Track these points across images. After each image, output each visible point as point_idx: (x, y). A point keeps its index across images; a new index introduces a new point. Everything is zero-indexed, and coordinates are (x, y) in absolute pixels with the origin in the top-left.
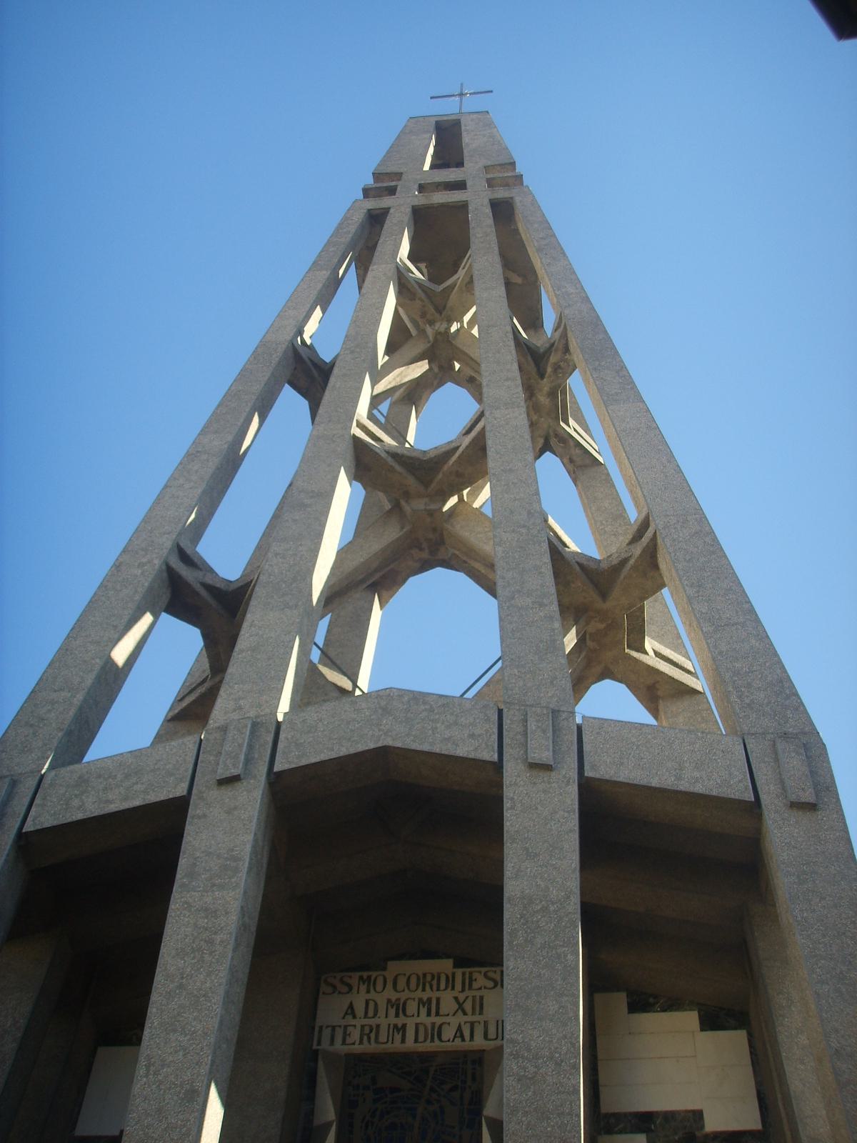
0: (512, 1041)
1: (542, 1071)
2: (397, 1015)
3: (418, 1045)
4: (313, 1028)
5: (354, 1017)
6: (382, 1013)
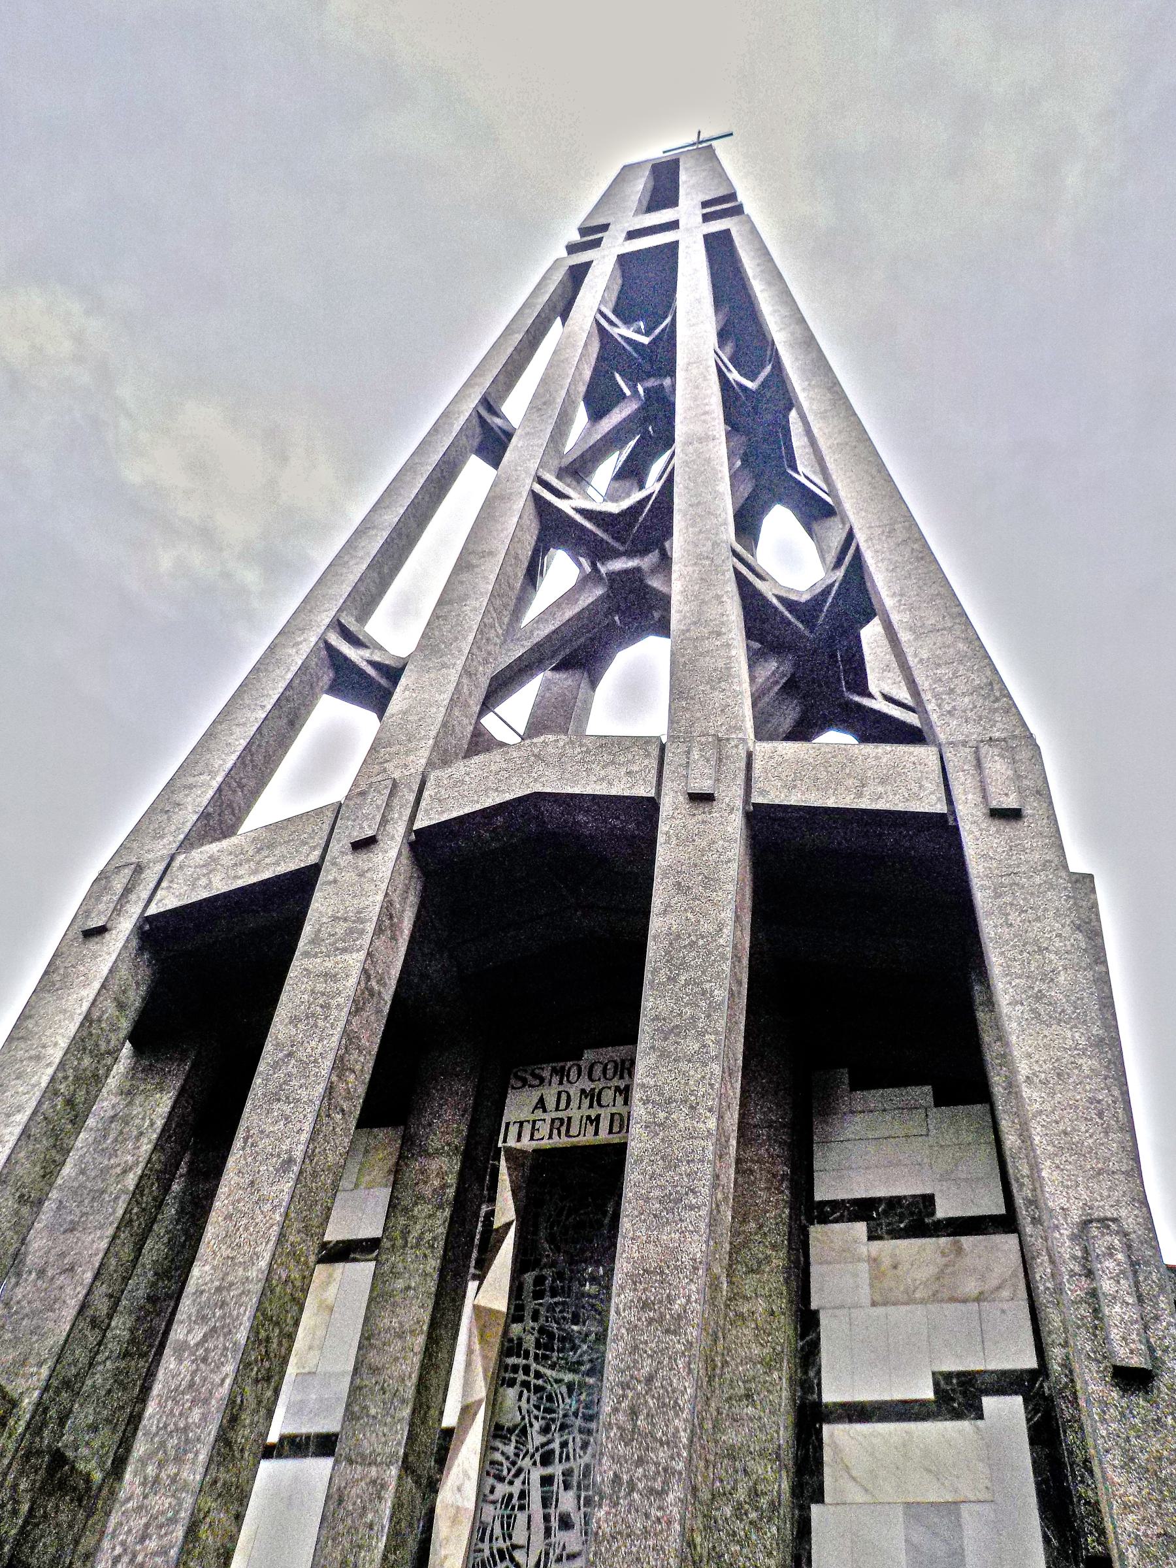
2: (591, 1106)
3: (611, 1136)
5: (545, 1111)
6: (574, 1104)
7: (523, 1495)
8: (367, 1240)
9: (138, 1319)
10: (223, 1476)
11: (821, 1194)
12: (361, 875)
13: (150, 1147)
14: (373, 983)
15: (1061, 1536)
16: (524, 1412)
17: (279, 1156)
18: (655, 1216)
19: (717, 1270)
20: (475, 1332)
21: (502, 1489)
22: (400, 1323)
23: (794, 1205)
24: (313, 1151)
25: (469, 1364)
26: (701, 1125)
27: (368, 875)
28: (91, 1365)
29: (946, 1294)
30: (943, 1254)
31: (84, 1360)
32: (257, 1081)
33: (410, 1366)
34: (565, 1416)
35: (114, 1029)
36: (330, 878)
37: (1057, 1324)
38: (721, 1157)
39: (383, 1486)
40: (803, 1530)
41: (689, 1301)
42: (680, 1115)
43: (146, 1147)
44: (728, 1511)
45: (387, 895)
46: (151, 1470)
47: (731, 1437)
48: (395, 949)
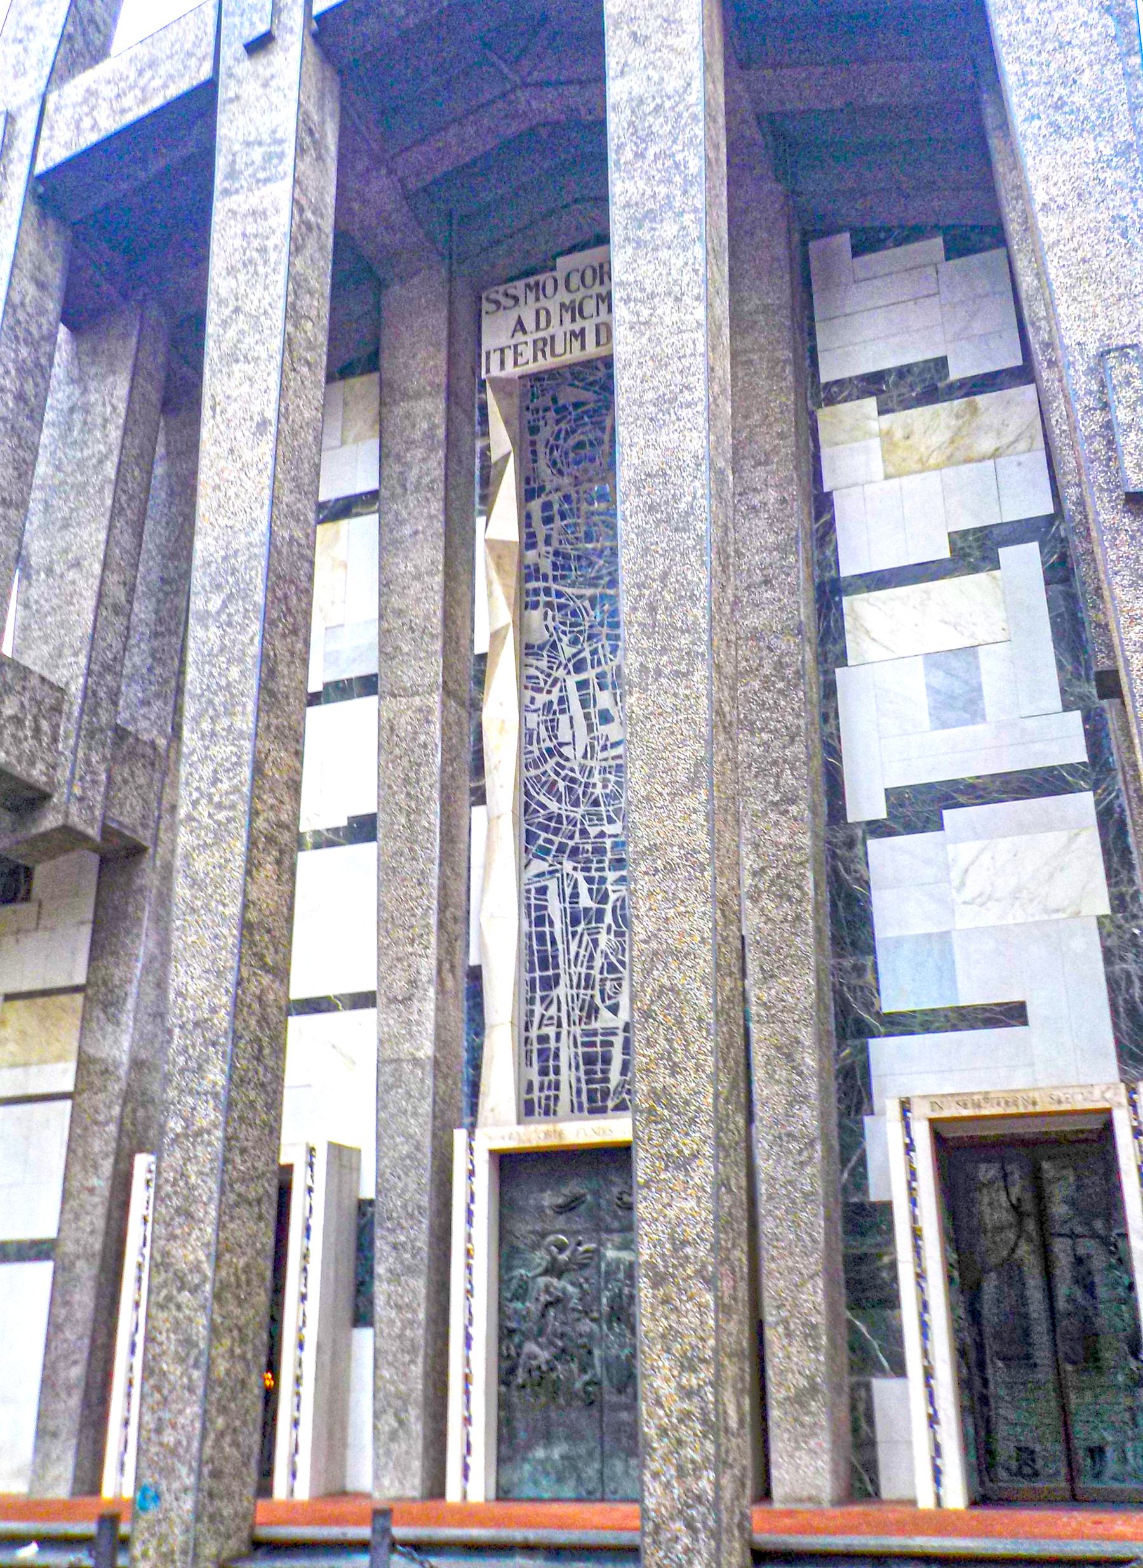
0: (622, 284)
1: (659, 312)
2: (573, 320)
4: (480, 356)
5: (525, 332)
6: (555, 320)
7: (562, 700)
8: (366, 494)
9: (159, 601)
10: (274, 721)
11: (826, 375)
12: (265, 85)
13: (119, 433)
14: (309, 215)
15: (1076, 660)
16: (551, 629)
17: (251, 418)
18: (651, 419)
19: (721, 464)
20: (492, 565)
21: (541, 699)
22: (415, 567)
23: (801, 396)
24: (287, 409)
25: (490, 595)
26: (688, 316)
27: (273, 83)
28: (125, 649)
29: (960, 455)
30: (957, 417)
31: (117, 645)
32: (210, 345)
33: (434, 604)
34: (591, 627)
35: (42, 312)
36: (231, 94)
37: (1072, 465)
38: (714, 349)
39: (430, 711)
40: (829, 690)
41: (694, 498)
42: (666, 309)
43: (115, 434)
44: (756, 685)
45: (299, 104)
46: (206, 726)
47: (754, 620)
48: (324, 171)
